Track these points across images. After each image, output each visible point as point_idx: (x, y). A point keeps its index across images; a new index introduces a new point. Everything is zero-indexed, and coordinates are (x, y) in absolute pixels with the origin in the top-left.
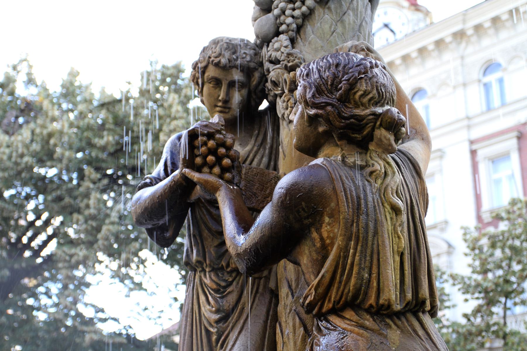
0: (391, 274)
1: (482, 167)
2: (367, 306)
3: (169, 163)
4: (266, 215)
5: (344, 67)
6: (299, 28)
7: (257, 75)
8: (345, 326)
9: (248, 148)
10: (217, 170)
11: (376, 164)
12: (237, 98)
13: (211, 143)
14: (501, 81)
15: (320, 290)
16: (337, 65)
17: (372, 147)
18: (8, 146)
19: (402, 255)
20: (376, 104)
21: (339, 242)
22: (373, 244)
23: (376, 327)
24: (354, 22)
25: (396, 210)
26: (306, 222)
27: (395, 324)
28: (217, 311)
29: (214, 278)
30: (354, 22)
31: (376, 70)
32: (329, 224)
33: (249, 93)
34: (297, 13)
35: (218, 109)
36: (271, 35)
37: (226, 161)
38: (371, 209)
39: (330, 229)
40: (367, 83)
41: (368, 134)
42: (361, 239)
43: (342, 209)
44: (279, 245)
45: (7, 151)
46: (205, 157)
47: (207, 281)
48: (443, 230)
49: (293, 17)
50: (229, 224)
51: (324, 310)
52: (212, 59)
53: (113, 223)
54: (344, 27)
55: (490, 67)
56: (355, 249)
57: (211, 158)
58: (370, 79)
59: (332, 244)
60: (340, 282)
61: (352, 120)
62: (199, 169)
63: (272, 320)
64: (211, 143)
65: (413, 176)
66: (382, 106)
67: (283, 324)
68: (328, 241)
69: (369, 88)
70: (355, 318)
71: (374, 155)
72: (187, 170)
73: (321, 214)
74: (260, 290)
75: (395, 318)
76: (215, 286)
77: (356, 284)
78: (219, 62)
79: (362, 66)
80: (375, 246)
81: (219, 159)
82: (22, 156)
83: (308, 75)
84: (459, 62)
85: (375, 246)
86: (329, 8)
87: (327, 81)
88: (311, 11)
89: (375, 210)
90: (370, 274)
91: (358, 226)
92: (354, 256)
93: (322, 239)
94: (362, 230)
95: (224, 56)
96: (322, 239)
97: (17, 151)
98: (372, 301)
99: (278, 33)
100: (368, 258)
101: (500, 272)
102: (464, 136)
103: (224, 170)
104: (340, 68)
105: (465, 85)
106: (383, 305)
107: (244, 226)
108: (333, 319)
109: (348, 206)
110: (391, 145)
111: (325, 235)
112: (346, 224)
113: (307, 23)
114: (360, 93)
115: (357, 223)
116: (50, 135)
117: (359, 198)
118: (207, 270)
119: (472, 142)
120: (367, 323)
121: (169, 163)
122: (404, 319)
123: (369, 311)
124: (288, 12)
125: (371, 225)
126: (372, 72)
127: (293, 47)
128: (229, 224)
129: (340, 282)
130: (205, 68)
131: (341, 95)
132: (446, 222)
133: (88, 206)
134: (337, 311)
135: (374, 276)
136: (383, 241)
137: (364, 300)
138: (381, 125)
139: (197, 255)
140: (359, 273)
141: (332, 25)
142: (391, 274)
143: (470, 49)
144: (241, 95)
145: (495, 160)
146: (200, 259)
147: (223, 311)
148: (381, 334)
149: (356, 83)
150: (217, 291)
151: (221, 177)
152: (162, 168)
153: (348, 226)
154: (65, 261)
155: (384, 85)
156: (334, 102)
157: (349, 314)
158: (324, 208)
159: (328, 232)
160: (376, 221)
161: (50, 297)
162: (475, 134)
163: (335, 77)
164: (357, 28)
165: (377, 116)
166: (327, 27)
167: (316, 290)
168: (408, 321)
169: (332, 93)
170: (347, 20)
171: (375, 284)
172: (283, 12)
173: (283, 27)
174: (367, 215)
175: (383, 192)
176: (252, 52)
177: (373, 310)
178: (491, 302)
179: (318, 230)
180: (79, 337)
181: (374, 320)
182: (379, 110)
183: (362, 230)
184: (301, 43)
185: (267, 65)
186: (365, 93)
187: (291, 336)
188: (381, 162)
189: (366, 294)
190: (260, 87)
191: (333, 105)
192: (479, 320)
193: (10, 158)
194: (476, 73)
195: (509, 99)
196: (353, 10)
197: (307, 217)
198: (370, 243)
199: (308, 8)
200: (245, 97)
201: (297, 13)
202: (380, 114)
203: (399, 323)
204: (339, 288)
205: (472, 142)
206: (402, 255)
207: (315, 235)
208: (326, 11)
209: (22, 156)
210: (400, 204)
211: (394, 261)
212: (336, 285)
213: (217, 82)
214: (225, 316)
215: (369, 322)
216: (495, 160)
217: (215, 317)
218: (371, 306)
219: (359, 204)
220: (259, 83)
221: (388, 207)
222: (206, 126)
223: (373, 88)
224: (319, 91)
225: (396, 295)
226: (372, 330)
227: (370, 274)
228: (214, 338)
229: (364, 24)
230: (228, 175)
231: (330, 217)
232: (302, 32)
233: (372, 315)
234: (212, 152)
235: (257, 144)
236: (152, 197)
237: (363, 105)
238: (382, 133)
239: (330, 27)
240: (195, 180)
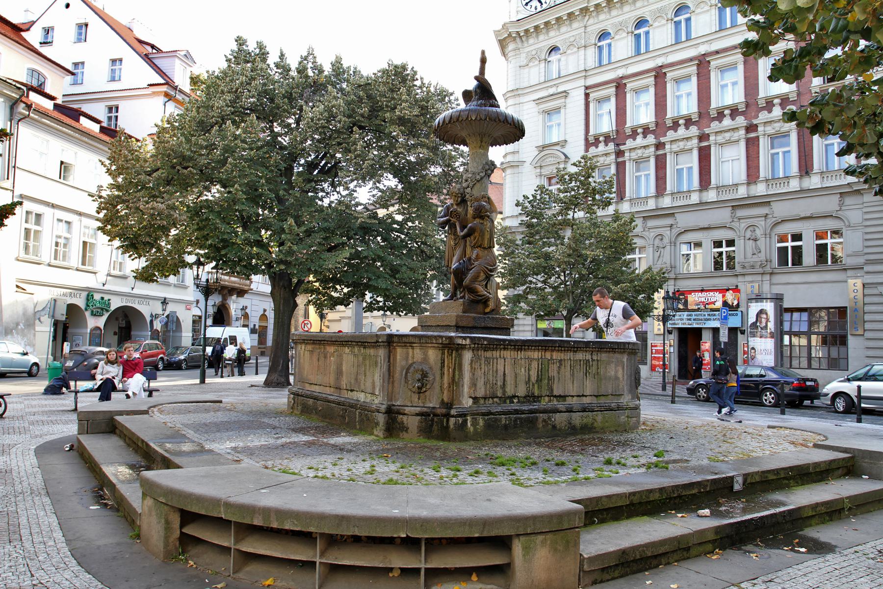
0: (486, 242)
1: (591, 105)
4: (466, 230)
14: (610, 45)
44: (468, 235)
48: (563, 146)
50: (458, 229)
55: (604, 35)
63: (465, 246)
84: (583, 30)
101: (573, 193)
102: (581, 82)
105: (585, 47)
119: (587, 88)
128: (458, 229)
132: (566, 141)
133: (356, 150)
142: (486, 242)
143: (591, 21)
145: (599, 101)
162: (590, 82)
178: (568, 209)
192: (560, 218)
194: (593, 39)
195: (613, 60)
205: (587, 88)
209: (319, 119)
216: (599, 101)
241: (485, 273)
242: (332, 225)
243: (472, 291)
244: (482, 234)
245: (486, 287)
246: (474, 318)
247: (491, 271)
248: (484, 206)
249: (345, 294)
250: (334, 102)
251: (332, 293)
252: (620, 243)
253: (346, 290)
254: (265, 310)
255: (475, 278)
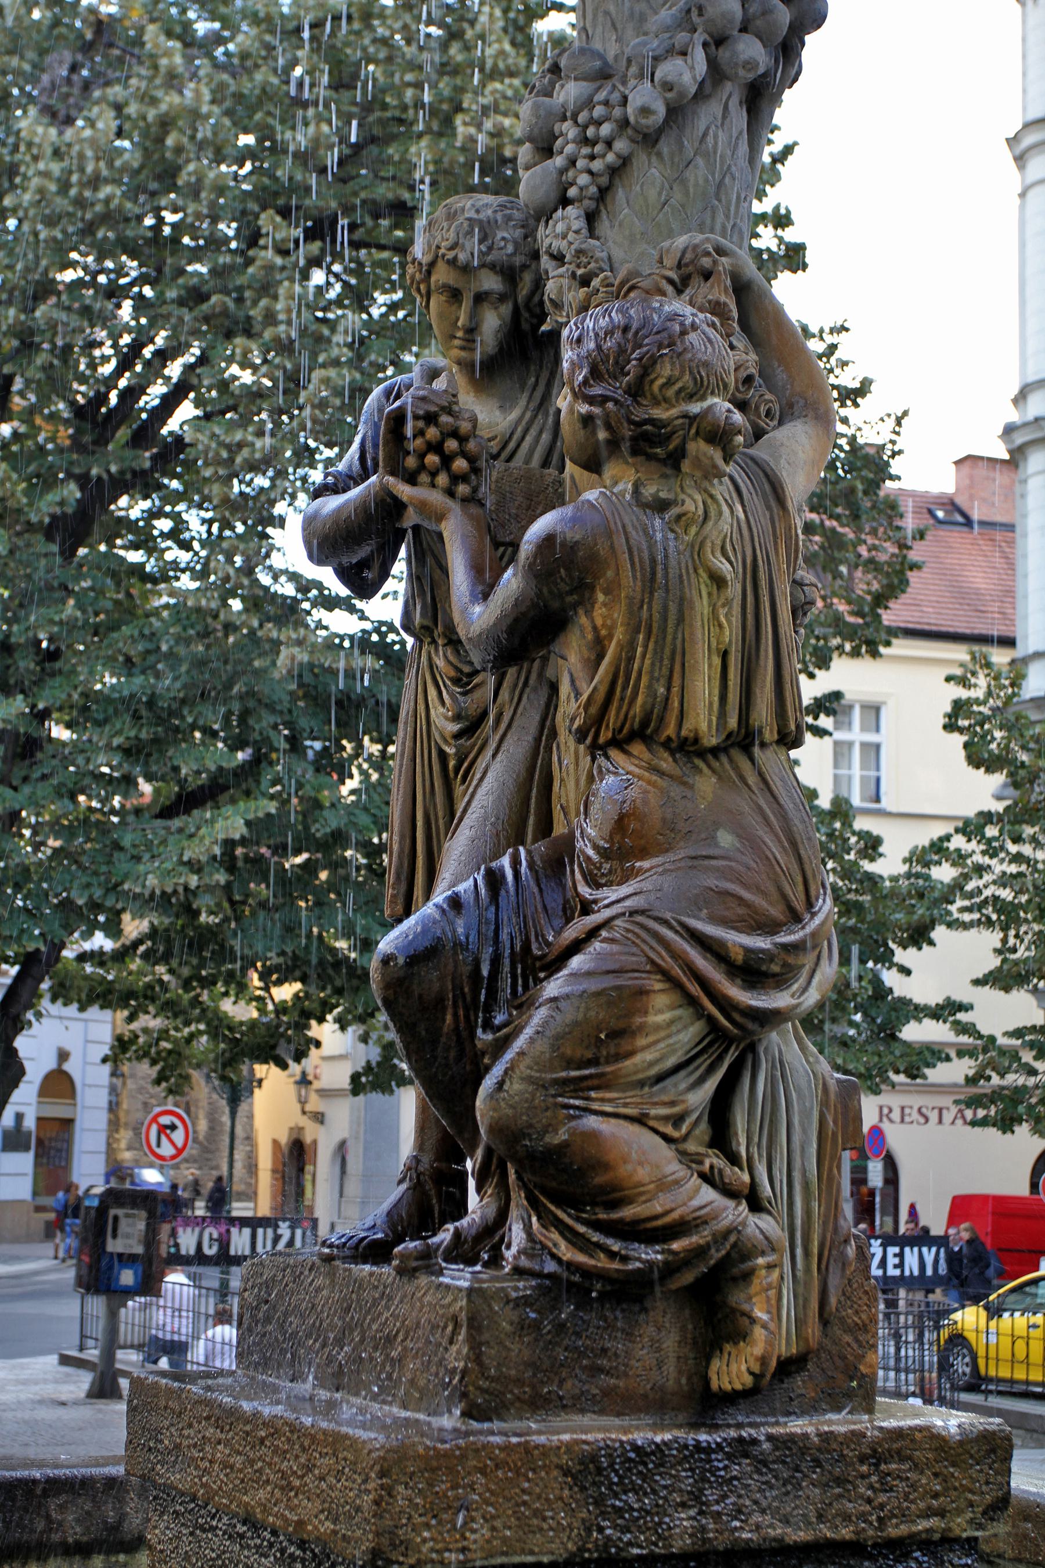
2: (663, 738)
3: (369, 445)
5: (637, 333)
6: (604, 193)
7: (528, 278)
8: (632, 768)
9: (514, 415)
10: (442, 479)
11: (688, 501)
12: (492, 322)
13: (432, 433)
15: (593, 710)
16: (626, 329)
17: (686, 466)
18: (57, 154)
19: (725, 655)
20: (691, 397)
21: (619, 634)
22: (675, 638)
23: (677, 771)
24: (707, 180)
25: (718, 581)
26: (569, 599)
27: (709, 766)
28: (457, 718)
29: (451, 658)
30: (707, 180)
31: (693, 337)
32: (605, 605)
33: (516, 312)
34: (597, 165)
35: (457, 342)
36: (552, 205)
37: (460, 464)
38: (673, 581)
39: (605, 613)
40: (673, 364)
41: (676, 449)
42: (655, 630)
43: (624, 582)
45: (56, 168)
46: (422, 456)
47: (440, 662)
49: (590, 172)
51: (602, 740)
52: (442, 251)
53: (336, 363)
54: (687, 193)
56: (646, 647)
57: (432, 459)
58: (680, 355)
59: (611, 636)
60: (622, 699)
61: (648, 427)
62: (411, 479)
64: (432, 433)
65: (769, 508)
66: (703, 398)
67: (563, 748)
68: (603, 632)
69: (677, 373)
70: (647, 756)
71: (688, 482)
72: (390, 480)
73: (592, 588)
74: (531, 682)
75: (710, 757)
76: (452, 673)
77: (644, 703)
78: (455, 258)
79: (665, 334)
80: (679, 642)
81: (447, 461)
82: (95, 182)
83: (579, 341)
85: (679, 642)
86: (659, 155)
87: (608, 356)
88: (625, 161)
89: (681, 582)
90: (669, 689)
91: (650, 609)
92: (644, 661)
93: (595, 628)
94: (656, 616)
95: (463, 248)
96: (595, 628)
97: (82, 170)
98: (670, 731)
99: (565, 202)
100: (666, 662)
103: (456, 479)
104: (630, 335)
106: (686, 739)
107: (485, 590)
108: (613, 753)
109: (634, 577)
110: (715, 466)
111: (599, 622)
112: (630, 605)
113: (617, 181)
114: (661, 381)
115: (650, 603)
116: (166, 123)
117: (653, 561)
118: (440, 642)
120: (664, 765)
121: (369, 445)
122: (724, 759)
123: (667, 744)
124: (581, 163)
125: (673, 608)
126: (683, 342)
127: (592, 233)
129: (622, 699)
130: (432, 264)
131: (629, 384)
133: (270, 318)
134: (619, 743)
135: (675, 690)
136: (692, 634)
137: (657, 730)
138: (697, 433)
139: (423, 615)
140: (650, 687)
141: (662, 189)
144: (500, 317)
146: (426, 623)
147: (467, 718)
148: (685, 784)
149: (655, 363)
150: (456, 681)
151: (451, 493)
152: (356, 462)
153: (634, 609)
154: (219, 462)
155: (706, 364)
156: (619, 395)
157: (637, 748)
158: (596, 577)
159: (604, 617)
160: (682, 599)
161: (186, 546)
163: (621, 351)
164: (712, 190)
165: (691, 419)
166: (652, 194)
167: (586, 709)
168: (731, 761)
169: (616, 378)
170: (692, 179)
171: (676, 704)
172: (573, 162)
173: (572, 192)
174: (667, 591)
175: (697, 549)
176: (519, 233)
177: (674, 745)
179: (589, 613)
180: (262, 654)
181: (675, 761)
182: (695, 408)
183: (656, 616)
184: (607, 223)
185: (545, 261)
186: (670, 382)
187: (572, 767)
188: (698, 498)
189: (661, 719)
190: (536, 299)
191: (616, 402)
193: (64, 186)
196: (706, 155)
197: (571, 593)
198: (669, 638)
199: (618, 156)
200: (508, 319)
201: (597, 165)
202: (696, 416)
203: (716, 764)
204: (620, 708)
206: (725, 655)
207: (583, 620)
208: (654, 159)
209: (95, 182)
210: (725, 567)
211: (710, 666)
212: (615, 704)
213: (455, 295)
214: (471, 726)
215: (666, 763)
217: (454, 727)
218: (669, 739)
219: (654, 573)
220: (533, 293)
221: (704, 575)
222: (423, 399)
223: (682, 372)
224: (595, 374)
225: (710, 721)
226: (670, 776)
227: (669, 689)
228: (452, 763)
229: (727, 180)
230: (462, 489)
231: (606, 594)
232: (609, 199)
233: (672, 753)
234: (436, 447)
235: (532, 406)
236: (339, 510)
237: (666, 400)
238: (698, 447)
239: (660, 194)
240: (405, 499)
241: (693, 994)
242: (168, 684)
243: (567, 1182)
244: (661, 625)
245: (720, 1137)
246: (588, 1470)
247: (753, 972)
248: (673, 338)
249: (281, 1009)
250: (169, 100)
251: (227, 1006)
252: (163, 893)
253: (285, 992)
254: (63, 1056)
255: (595, 1052)
